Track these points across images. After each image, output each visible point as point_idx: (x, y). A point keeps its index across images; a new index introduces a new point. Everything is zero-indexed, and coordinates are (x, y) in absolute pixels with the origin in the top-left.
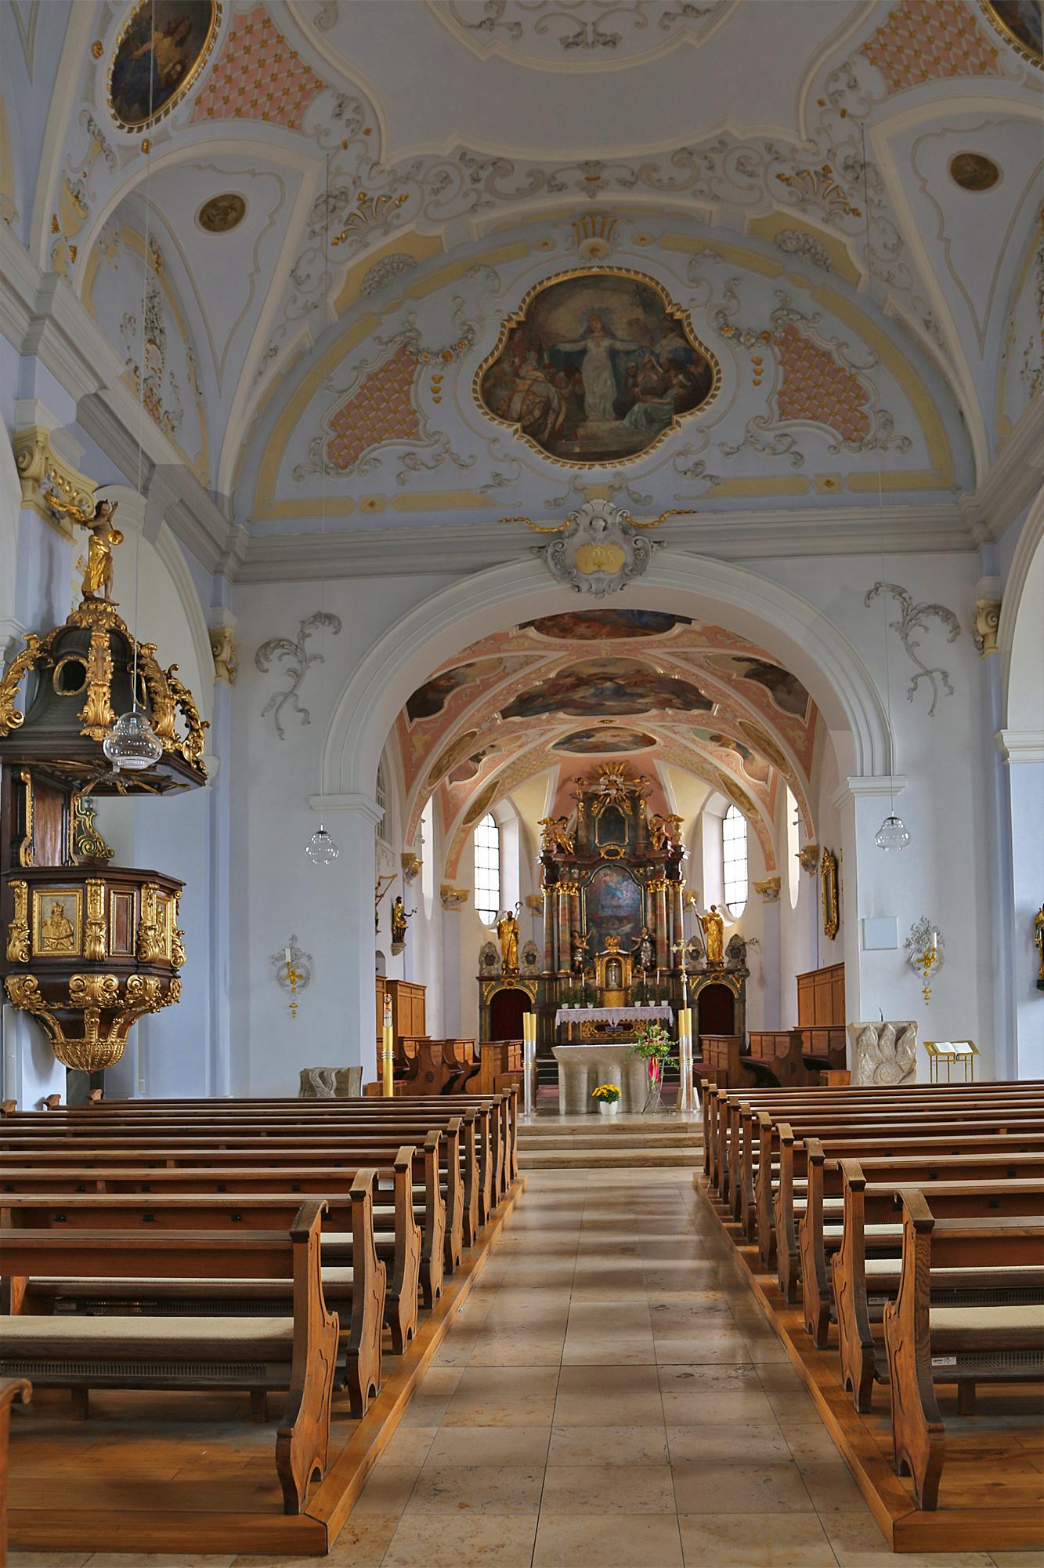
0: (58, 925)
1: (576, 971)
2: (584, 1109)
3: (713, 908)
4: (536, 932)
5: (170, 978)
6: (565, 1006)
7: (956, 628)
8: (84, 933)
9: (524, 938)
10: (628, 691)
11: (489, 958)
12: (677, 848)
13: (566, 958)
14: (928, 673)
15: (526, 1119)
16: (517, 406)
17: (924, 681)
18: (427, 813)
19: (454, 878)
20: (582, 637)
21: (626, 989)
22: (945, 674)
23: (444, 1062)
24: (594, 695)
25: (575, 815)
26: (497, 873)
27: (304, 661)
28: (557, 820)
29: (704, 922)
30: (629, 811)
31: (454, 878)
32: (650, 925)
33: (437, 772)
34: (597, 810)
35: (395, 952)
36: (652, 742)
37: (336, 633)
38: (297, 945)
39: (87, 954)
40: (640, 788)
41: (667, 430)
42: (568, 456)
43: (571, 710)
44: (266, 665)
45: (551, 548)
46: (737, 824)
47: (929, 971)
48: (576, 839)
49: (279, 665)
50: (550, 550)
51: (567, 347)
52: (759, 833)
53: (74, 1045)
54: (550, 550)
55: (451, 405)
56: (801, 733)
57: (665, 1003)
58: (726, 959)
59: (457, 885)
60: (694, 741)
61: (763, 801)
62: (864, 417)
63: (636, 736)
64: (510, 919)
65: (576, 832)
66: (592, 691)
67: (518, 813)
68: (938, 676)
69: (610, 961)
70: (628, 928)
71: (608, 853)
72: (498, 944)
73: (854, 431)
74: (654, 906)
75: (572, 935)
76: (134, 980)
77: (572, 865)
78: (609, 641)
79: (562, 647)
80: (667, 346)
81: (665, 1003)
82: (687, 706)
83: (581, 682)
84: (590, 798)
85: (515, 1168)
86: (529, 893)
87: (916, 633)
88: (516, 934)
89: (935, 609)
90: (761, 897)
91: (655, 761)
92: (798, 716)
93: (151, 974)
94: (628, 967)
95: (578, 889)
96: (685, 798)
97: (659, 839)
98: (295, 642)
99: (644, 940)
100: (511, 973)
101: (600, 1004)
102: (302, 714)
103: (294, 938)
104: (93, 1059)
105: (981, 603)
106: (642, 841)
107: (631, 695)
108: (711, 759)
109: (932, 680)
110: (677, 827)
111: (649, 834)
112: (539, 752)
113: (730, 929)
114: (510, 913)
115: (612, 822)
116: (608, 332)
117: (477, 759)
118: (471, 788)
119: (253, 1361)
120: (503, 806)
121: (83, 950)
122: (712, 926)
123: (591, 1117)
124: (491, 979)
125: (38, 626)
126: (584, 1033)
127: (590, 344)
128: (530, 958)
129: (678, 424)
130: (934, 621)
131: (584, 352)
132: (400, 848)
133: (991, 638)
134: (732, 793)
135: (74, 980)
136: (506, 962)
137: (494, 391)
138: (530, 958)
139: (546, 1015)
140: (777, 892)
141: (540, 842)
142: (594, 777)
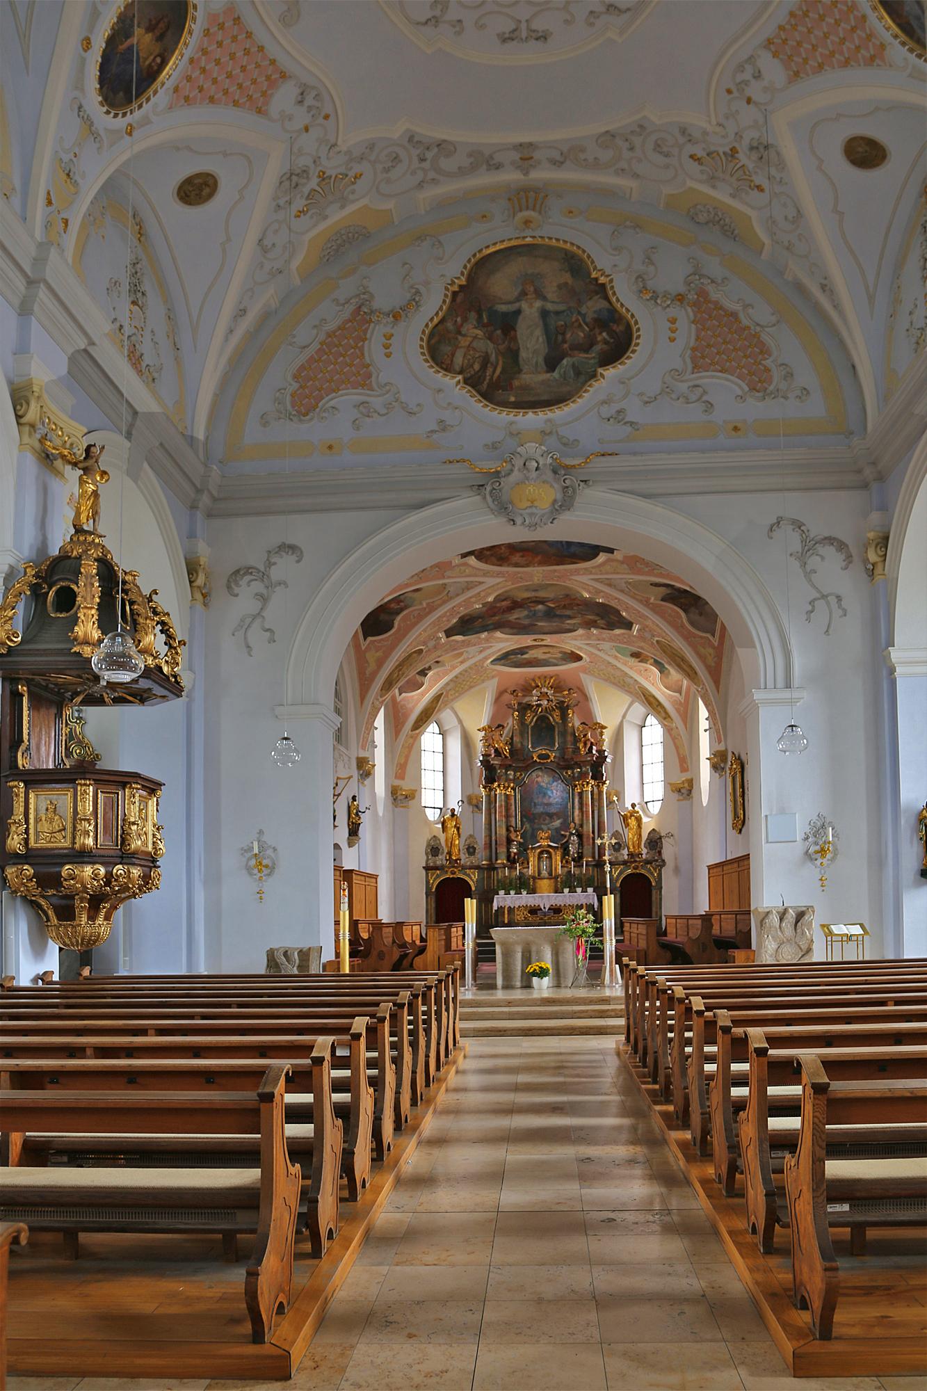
0: (51, 821)
1: (512, 861)
2: (518, 984)
3: (633, 805)
4: (476, 827)
5: (151, 868)
6: (502, 892)
7: (849, 557)
8: (75, 827)
9: (465, 832)
10: (558, 613)
11: (434, 850)
12: (601, 752)
13: (502, 850)
14: (824, 597)
15: (467, 993)
16: (459, 360)
17: (820, 604)
18: (380, 722)
19: (403, 778)
20: (516, 565)
21: (556, 877)
22: (839, 598)
23: (394, 942)
24: (527, 617)
25: (511, 723)
26: (441, 774)
27: (270, 586)
28: (495, 727)
29: (625, 818)
30: (558, 720)
31: (403, 778)
32: (577, 821)
33: (388, 685)
34: (530, 718)
35: (350, 845)
36: (579, 658)
37: (298, 562)
38: (264, 838)
39: (77, 846)
40: (568, 699)
41: (592, 382)
42: (504, 404)
43: (507, 630)
44: (236, 590)
45: (489, 486)
46: (654, 731)
47: (825, 861)
48: (511, 744)
49: (248, 590)
50: (489, 488)
51: (503, 308)
52: (674, 739)
53: (66, 927)
54: (489, 488)
55: (401, 359)
56: (711, 651)
57: (590, 890)
58: (644, 851)
59: (406, 785)
60: (616, 657)
61: (678, 710)
62: (768, 370)
63: (565, 653)
64: (453, 815)
65: (512, 738)
66: (526, 613)
67: (460, 722)
68: (832, 600)
69: (541, 853)
70: (557, 823)
71: (540, 757)
72: (442, 837)
73: (758, 382)
74: (581, 804)
75: (508, 830)
76: (119, 869)
77: (508, 767)
78: (541, 569)
79: (499, 574)
80: (593, 307)
81: (590, 890)
82: (610, 626)
83: (516, 605)
84: (524, 708)
85: (458, 1036)
86: (470, 792)
87: (813, 561)
88: (458, 829)
89: (830, 540)
90: (676, 795)
91: (582, 675)
92: (708, 635)
93: (134, 864)
94: (557, 858)
95: (513, 789)
96: (608, 708)
97: (585, 744)
98: (262, 569)
99: (572, 834)
100: (454, 863)
101: (532, 891)
102: (268, 634)
103: (261, 832)
104: (83, 939)
105: (871, 535)
106: (570, 746)
107: (561, 616)
108: (631, 673)
109: (828, 603)
110: (602, 734)
111: (576, 740)
112: (478, 667)
113: (648, 824)
114: (453, 810)
115: (544, 729)
116: (540, 295)
117: (423, 673)
118: (419, 699)
119: (224, 1208)
120: (446, 715)
121: (74, 843)
122: (632, 822)
123: (525, 991)
124: (436, 868)
125: (34, 556)
126: (519, 917)
127: (524, 305)
128: (471, 850)
129: (602, 376)
130: (829, 551)
131: (518, 312)
132: (355, 752)
133: (880, 566)
134: (650, 704)
135: (66, 870)
136: (449, 853)
137: (438, 347)
138: (471, 850)
139: (485, 900)
140: (690, 791)
141: (480, 747)
142: (527, 690)
